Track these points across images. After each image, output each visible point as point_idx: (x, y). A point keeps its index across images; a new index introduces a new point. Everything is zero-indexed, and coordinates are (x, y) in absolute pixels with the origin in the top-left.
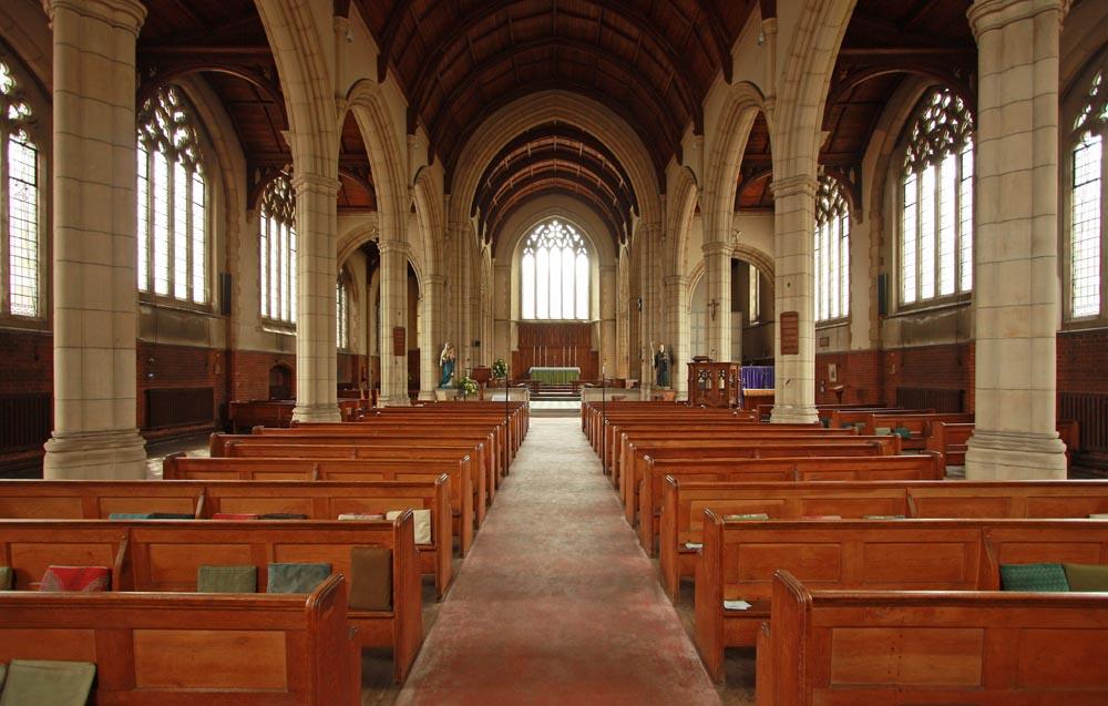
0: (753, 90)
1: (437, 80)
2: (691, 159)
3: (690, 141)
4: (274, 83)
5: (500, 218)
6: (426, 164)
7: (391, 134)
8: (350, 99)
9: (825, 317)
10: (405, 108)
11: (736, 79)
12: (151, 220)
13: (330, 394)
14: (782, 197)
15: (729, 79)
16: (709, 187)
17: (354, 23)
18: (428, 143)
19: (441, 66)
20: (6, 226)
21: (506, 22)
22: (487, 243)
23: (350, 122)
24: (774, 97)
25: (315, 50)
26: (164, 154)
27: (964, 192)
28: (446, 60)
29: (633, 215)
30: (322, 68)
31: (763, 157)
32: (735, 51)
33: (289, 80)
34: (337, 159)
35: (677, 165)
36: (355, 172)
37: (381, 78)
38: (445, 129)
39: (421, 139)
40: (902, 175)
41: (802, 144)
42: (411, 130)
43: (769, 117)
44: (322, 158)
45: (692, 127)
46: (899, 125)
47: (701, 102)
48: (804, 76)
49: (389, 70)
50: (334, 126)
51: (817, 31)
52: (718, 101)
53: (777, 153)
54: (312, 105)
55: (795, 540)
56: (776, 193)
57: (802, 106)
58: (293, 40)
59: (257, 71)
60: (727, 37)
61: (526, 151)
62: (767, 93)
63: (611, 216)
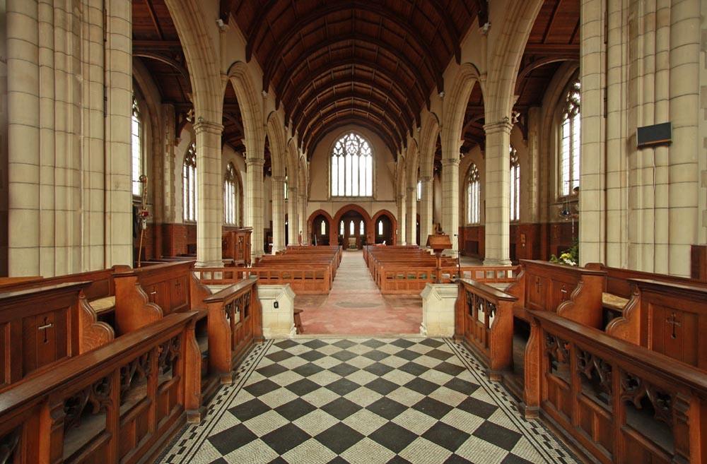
0: (473, 68)
1: (281, 59)
2: (435, 107)
3: (435, 97)
4: (183, 63)
5: (317, 145)
6: (274, 110)
7: (196, 9)
8: (230, 74)
9: (650, 123)
10: (274, 98)
11: (463, 61)
12: (188, 191)
13: (217, 253)
14: (491, 133)
15: (459, 62)
16: (446, 125)
17: (232, 28)
18: (284, 113)
19: (284, 51)
20: (458, 322)
21: (325, 24)
22: (304, 153)
23: (230, 85)
24: (486, 74)
25: (208, 46)
26: (137, 118)
27: (564, 165)
28: (287, 48)
29: (403, 147)
30: (215, 59)
31: (479, 107)
32: (462, 46)
33: (275, 155)
34: (222, 112)
35: (427, 111)
36: (232, 115)
37: (248, 59)
38: (284, 82)
39: (270, 96)
40: (561, 120)
41: (503, 106)
42: (265, 88)
43: (483, 87)
44: (212, 111)
45: (436, 89)
46: (559, 91)
47: (441, 73)
48: (503, 67)
49: (253, 55)
50: (221, 92)
51: (517, 22)
52: (452, 74)
53: (488, 107)
54: (207, 78)
55: (181, 198)
56: (487, 131)
57: (506, 65)
58: (189, 23)
59: (173, 57)
60: (458, 34)
61: (332, 90)
62: (482, 71)
63: (390, 142)
